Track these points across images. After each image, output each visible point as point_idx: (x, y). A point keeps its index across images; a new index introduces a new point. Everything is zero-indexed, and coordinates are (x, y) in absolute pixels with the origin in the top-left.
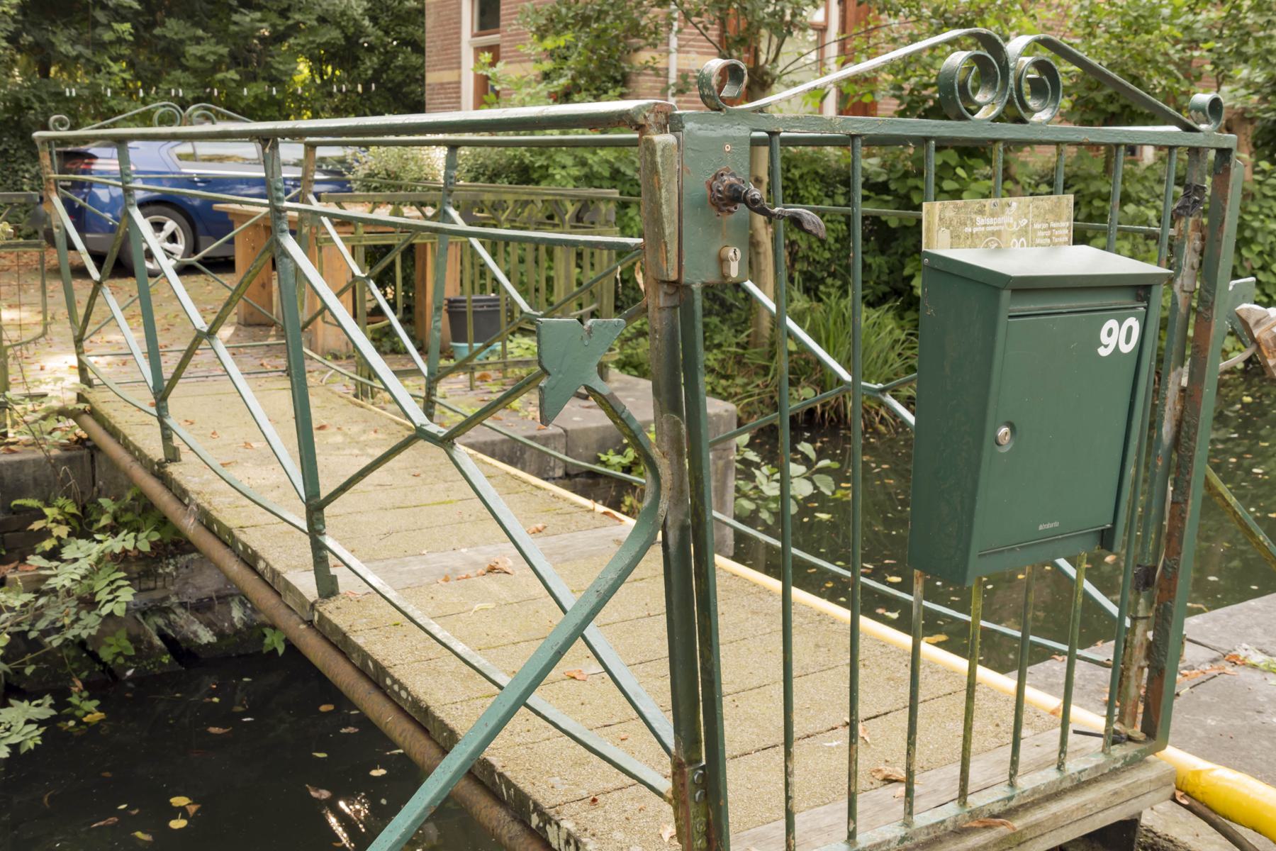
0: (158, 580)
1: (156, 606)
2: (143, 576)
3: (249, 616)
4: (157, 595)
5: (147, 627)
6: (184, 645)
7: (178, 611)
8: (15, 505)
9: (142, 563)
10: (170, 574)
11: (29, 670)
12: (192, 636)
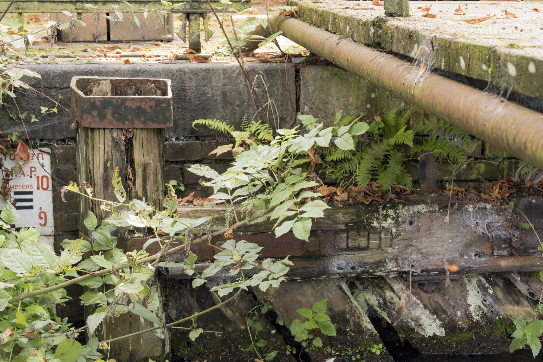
0: (372, 236)
1: (367, 272)
2: (352, 228)
3: (490, 306)
4: (370, 257)
5: (355, 303)
6: (402, 336)
7: (397, 286)
8: (197, 125)
9: (351, 210)
10: (388, 231)
11: (194, 335)
12: (413, 324)
